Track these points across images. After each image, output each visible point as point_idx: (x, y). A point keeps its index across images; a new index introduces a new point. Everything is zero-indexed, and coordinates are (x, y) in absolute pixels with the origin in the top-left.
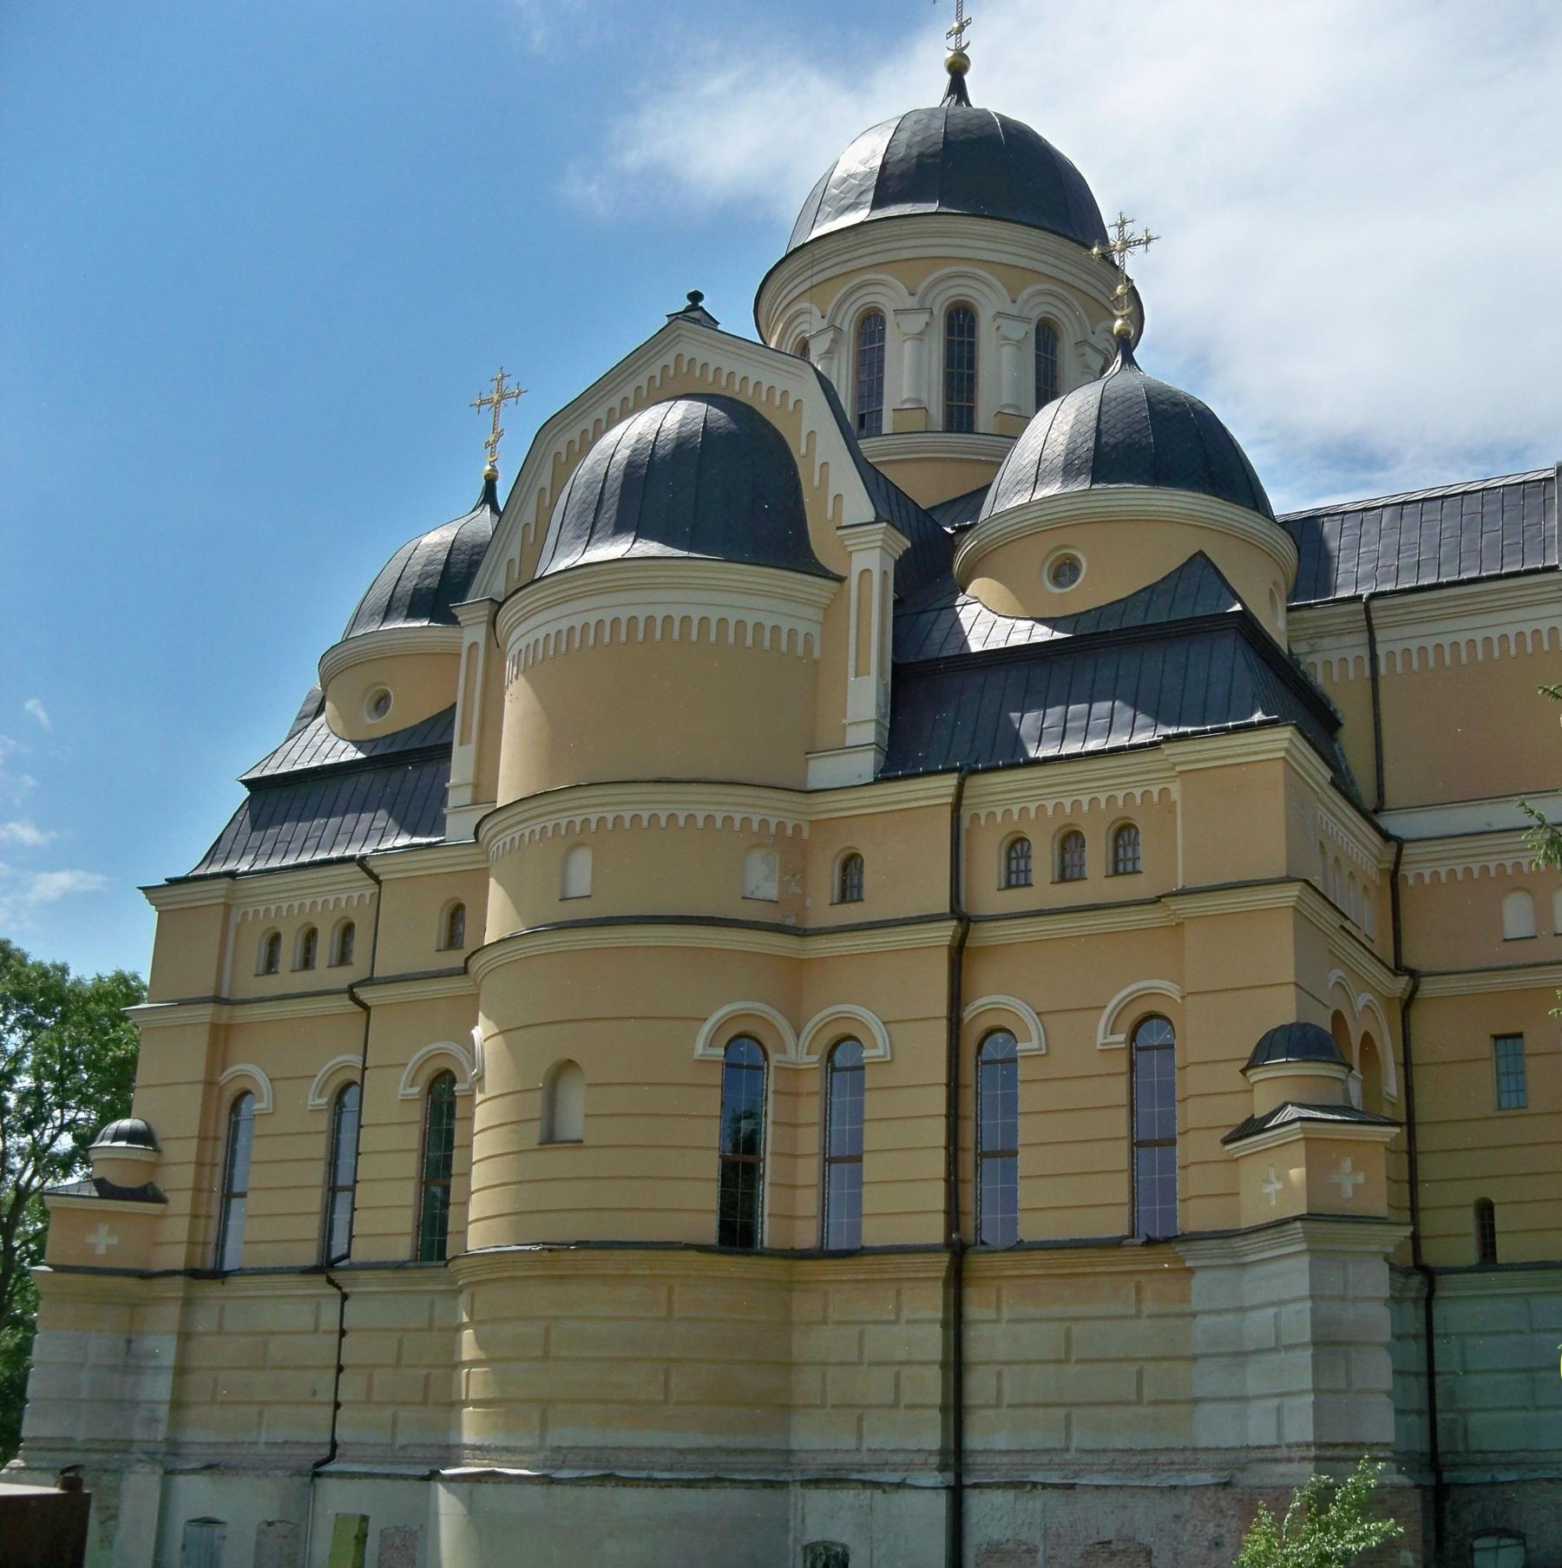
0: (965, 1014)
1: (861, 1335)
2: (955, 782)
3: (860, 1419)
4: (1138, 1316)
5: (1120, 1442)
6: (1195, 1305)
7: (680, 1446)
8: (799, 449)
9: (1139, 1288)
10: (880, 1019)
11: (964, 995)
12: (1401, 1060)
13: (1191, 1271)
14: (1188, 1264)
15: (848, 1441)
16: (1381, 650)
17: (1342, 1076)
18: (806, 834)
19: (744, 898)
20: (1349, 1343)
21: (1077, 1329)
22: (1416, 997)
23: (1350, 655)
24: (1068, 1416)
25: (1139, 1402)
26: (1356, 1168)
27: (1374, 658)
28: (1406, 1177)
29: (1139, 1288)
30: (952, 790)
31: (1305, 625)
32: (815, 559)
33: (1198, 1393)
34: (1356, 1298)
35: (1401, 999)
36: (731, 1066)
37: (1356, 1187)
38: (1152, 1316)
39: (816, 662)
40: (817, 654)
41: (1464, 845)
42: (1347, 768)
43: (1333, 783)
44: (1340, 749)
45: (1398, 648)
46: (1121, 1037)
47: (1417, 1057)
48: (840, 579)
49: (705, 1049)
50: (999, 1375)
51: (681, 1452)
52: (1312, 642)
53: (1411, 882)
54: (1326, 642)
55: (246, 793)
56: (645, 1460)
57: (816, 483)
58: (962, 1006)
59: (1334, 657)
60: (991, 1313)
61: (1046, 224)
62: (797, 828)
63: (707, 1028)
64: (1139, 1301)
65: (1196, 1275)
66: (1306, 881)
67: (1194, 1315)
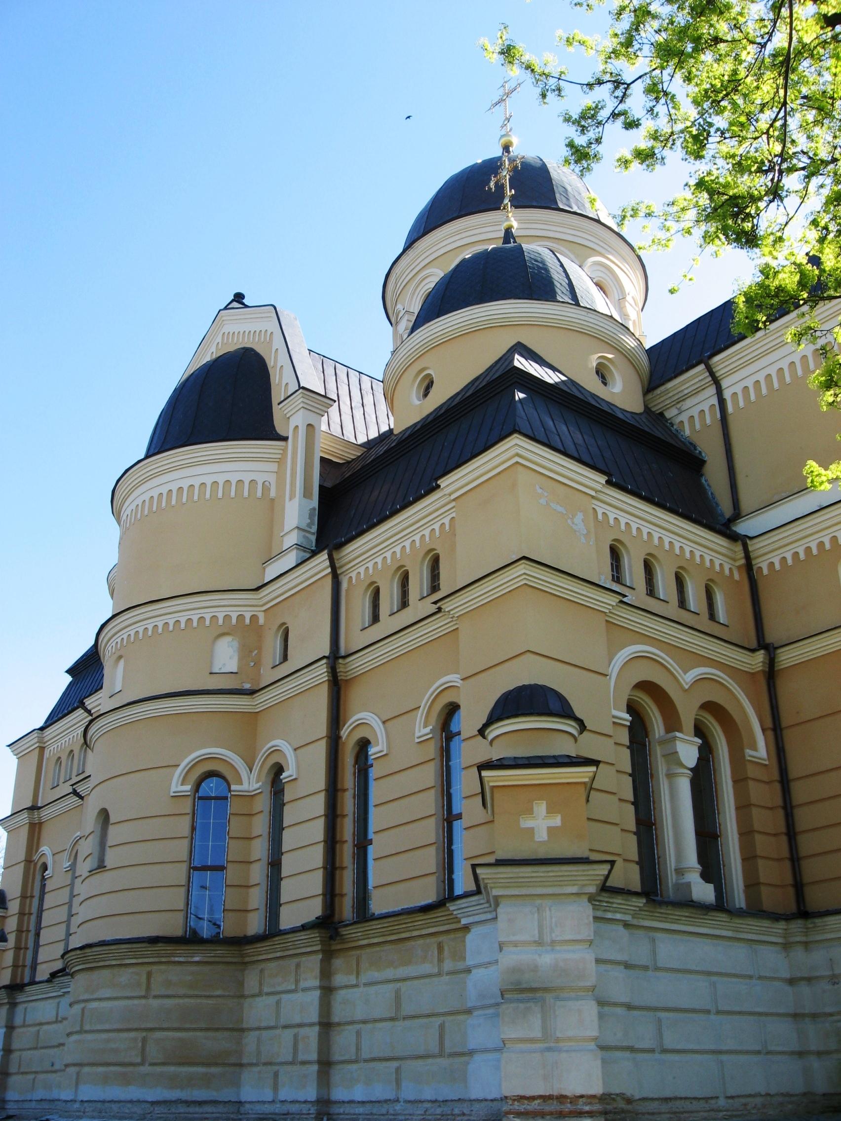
0: (342, 733)
1: (278, 1003)
2: (326, 556)
3: (276, 1075)
4: (439, 974)
5: (428, 1094)
6: (470, 962)
7: (150, 1099)
8: (270, 364)
9: (440, 948)
10: (290, 744)
11: (341, 718)
12: (769, 723)
13: (466, 928)
14: (464, 921)
15: (268, 1095)
16: (727, 395)
17: (575, 733)
18: (261, 621)
19: (211, 673)
20: (546, 990)
21: (404, 987)
22: (776, 669)
23: (706, 406)
24: (398, 1070)
25: (441, 1055)
26: (550, 811)
27: (722, 401)
28: (784, 830)
29: (440, 948)
30: (327, 563)
31: (671, 395)
32: (276, 431)
33: (472, 1045)
34: (553, 942)
35: (763, 671)
36: (199, 797)
37: (531, 830)
38: (449, 973)
39: (273, 500)
40: (273, 494)
41: (796, 530)
42: (712, 494)
43: (609, 483)
44: (706, 481)
45: (738, 388)
46: (188, 787)
47: (787, 719)
48: (285, 439)
49: (177, 787)
50: (358, 1033)
51: (153, 1103)
52: (678, 406)
53: (765, 571)
54: (689, 403)
55: (69, 679)
56: (127, 1111)
57: (277, 381)
58: (341, 723)
59: (695, 412)
60: (352, 980)
61: (535, 204)
62: (254, 618)
63: (178, 772)
64: (440, 960)
65: (472, 930)
66: (524, 558)
67: (468, 971)
